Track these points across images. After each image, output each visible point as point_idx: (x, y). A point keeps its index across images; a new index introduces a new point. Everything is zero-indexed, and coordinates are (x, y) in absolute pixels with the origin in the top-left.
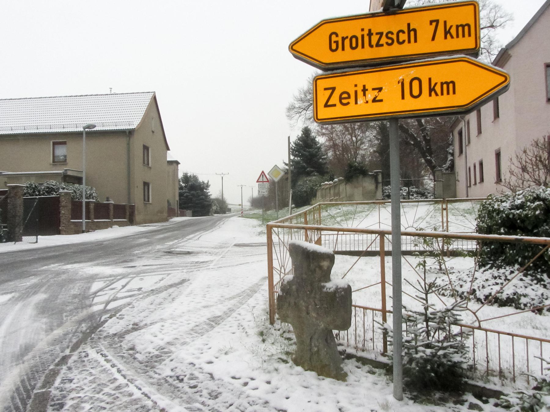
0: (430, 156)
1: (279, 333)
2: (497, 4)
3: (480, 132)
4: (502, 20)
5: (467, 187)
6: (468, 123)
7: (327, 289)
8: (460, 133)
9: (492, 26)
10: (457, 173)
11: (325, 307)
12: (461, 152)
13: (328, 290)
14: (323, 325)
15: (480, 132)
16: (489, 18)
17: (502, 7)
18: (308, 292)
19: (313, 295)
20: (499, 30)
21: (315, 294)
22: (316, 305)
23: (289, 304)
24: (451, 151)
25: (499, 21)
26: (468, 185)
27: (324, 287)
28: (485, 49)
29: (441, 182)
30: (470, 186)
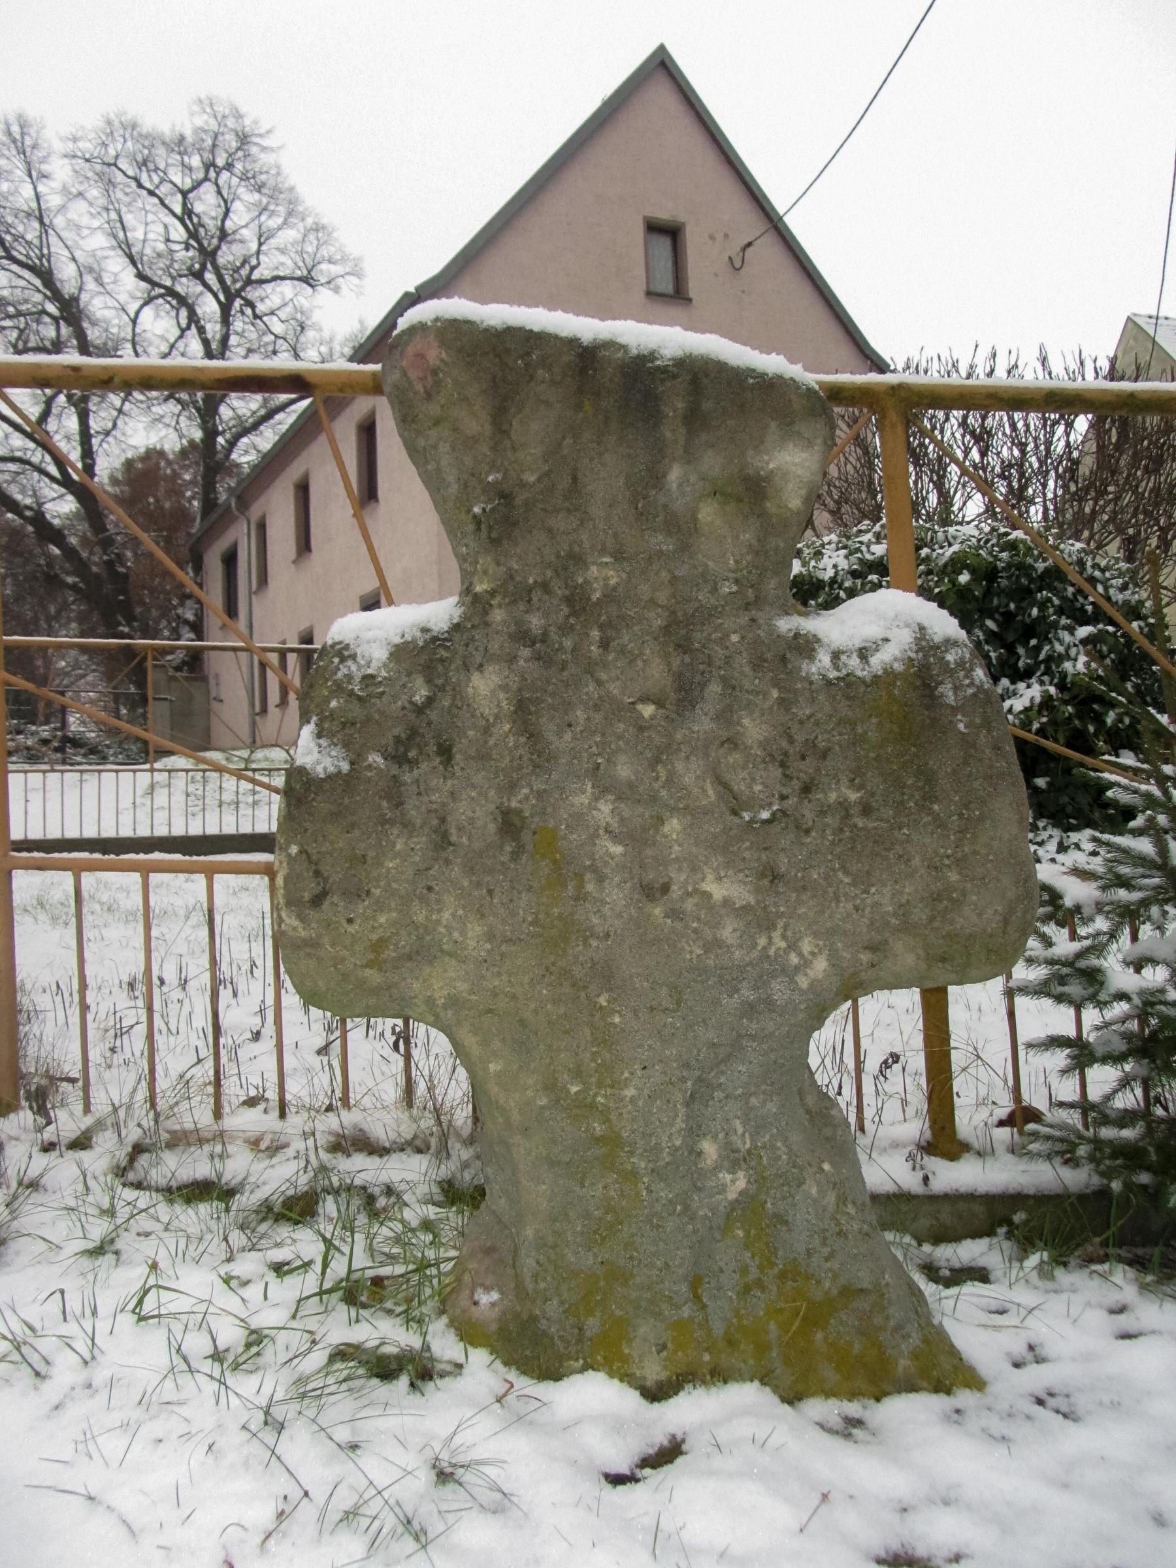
0: (129, 624)
1: (98, 1160)
2: (324, 221)
3: (304, 545)
4: (335, 269)
5: (254, 714)
6: (262, 527)
7: (836, 655)
8: (230, 560)
9: (308, 280)
10: (217, 676)
11: (843, 806)
12: (231, 609)
13: (854, 662)
14: (821, 965)
15: (304, 545)
16: (301, 253)
17: (335, 235)
18: (648, 710)
19: (703, 723)
20: (324, 293)
21: (726, 716)
22: (735, 803)
23: (442, 841)
24: (190, 616)
25: (325, 270)
26: (257, 710)
27: (806, 645)
28: (285, 339)
29: (167, 704)
30: (264, 710)
